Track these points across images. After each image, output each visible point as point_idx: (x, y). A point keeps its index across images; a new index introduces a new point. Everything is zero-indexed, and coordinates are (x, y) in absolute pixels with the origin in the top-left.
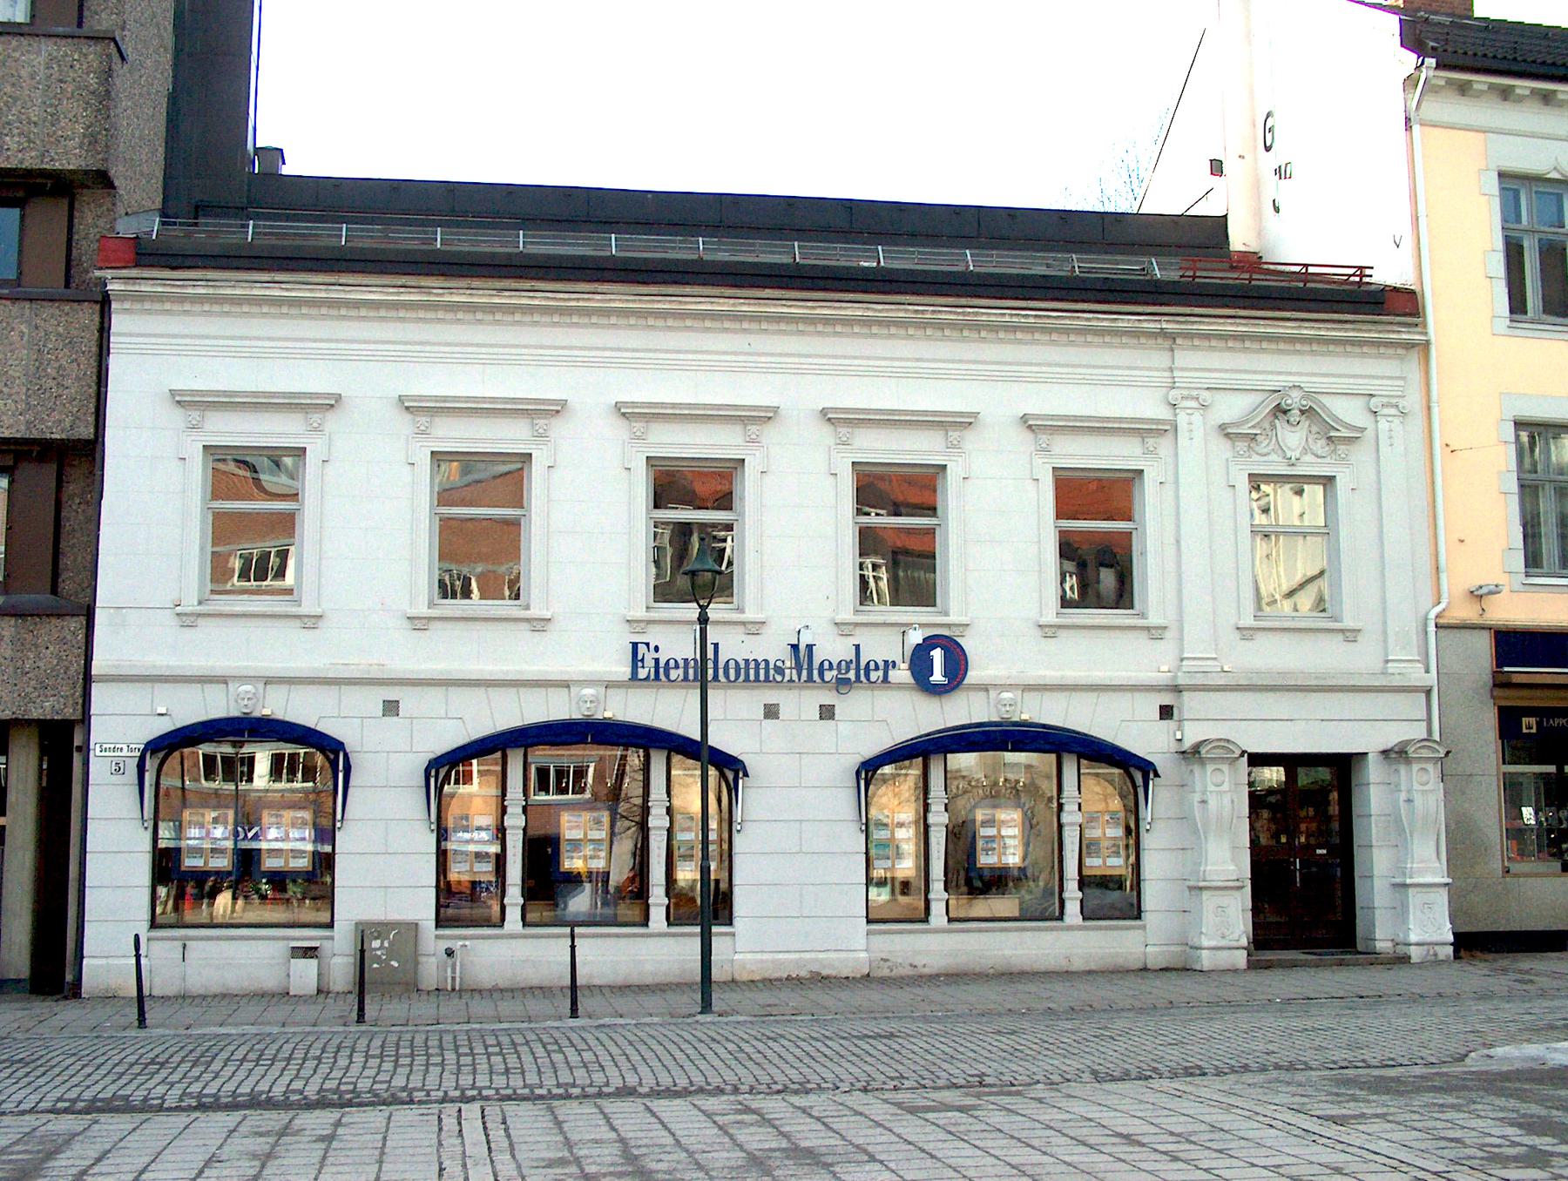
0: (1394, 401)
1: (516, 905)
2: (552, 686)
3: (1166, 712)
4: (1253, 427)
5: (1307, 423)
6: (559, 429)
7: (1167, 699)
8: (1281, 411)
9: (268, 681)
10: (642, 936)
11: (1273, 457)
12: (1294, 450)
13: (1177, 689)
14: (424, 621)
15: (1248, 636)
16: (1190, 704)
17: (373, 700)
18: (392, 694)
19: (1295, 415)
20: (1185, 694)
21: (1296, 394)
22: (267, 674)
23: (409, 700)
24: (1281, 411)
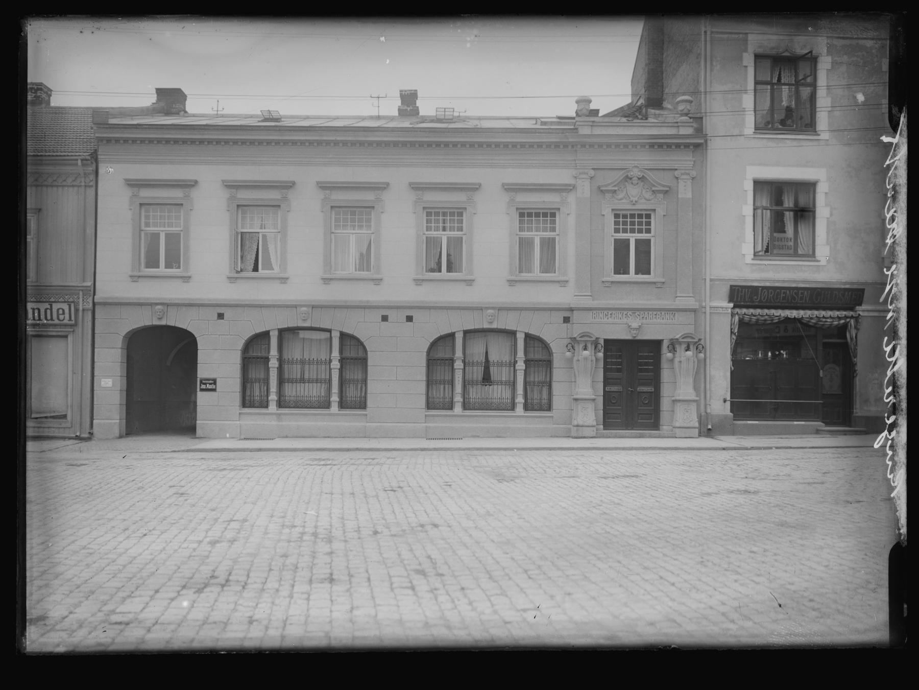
0: (687, 172)
1: (336, 401)
2: (510, 310)
3: (566, 320)
4: (615, 186)
5: (642, 184)
6: (195, 193)
7: (567, 314)
8: (628, 178)
9: (500, 309)
10: (265, 414)
11: (624, 201)
12: (634, 197)
13: (571, 310)
14: (137, 278)
15: (283, 281)
16: (576, 317)
17: (377, 315)
18: (221, 310)
19: (635, 180)
20: (574, 312)
21: (636, 170)
22: (313, 304)
23: (228, 313)
24: (628, 178)
